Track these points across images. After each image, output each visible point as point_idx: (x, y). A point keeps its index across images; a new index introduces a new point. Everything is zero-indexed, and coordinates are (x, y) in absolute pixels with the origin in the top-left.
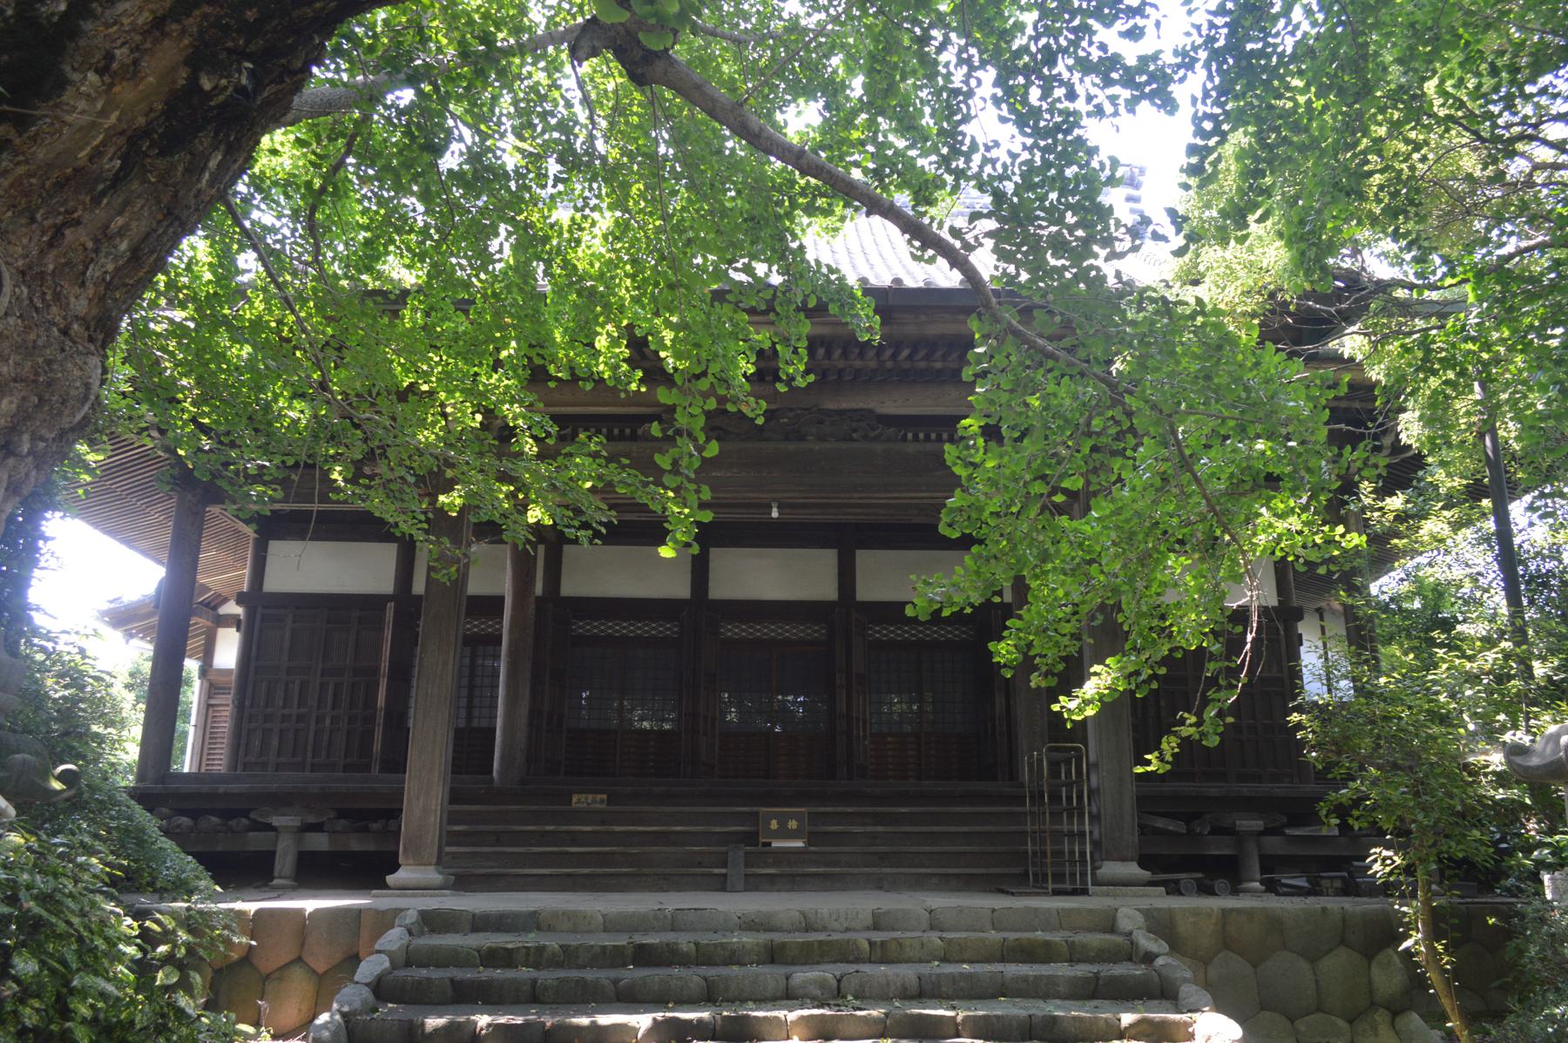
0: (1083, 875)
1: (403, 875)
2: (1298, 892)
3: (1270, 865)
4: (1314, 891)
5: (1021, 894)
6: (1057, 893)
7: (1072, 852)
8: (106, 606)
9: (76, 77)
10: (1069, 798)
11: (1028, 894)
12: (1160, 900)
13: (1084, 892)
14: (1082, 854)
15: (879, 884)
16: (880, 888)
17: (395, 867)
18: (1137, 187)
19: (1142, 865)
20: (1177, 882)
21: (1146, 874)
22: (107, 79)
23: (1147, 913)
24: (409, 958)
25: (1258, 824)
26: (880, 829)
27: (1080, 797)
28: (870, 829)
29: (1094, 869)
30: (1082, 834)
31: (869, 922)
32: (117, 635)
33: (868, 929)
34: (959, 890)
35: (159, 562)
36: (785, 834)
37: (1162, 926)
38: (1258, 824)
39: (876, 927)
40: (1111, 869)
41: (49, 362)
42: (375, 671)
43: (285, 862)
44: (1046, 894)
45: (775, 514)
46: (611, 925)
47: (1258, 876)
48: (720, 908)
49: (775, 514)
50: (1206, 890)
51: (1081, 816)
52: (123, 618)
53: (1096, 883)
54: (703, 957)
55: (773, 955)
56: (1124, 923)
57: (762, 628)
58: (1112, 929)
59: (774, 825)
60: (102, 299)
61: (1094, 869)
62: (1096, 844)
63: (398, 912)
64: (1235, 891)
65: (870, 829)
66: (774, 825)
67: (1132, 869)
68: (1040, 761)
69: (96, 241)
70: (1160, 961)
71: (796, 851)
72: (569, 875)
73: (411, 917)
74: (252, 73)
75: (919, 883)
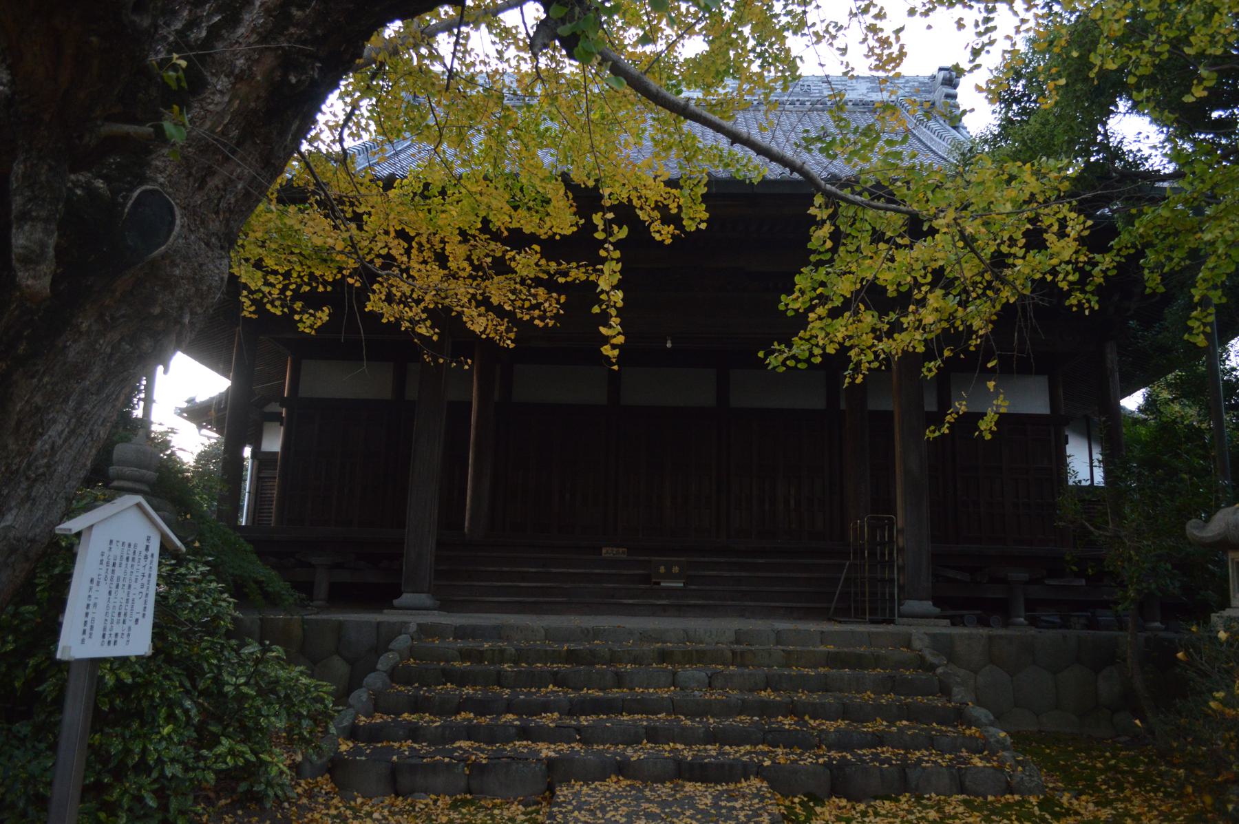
0: (892, 610)
1: (407, 598)
2: (1052, 625)
3: (1031, 605)
4: (1065, 625)
5: (845, 622)
6: (873, 622)
7: (884, 594)
8: (185, 405)
9: (215, 80)
10: (883, 554)
11: (852, 622)
12: (943, 628)
13: (891, 622)
14: (892, 595)
15: (742, 613)
16: (742, 616)
17: (399, 595)
18: (955, 87)
19: (935, 605)
20: (962, 616)
21: (938, 610)
22: (232, 79)
23: (933, 637)
24: (412, 652)
25: (1024, 576)
26: (743, 574)
27: (891, 554)
28: (735, 574)
29: (900, 605)
30: (892, 581)
31: (733, 638)
32: (191, 427)
33: (732, 643)
34: (800, 619)
35: (228, 377)
36: (669, 576)
37: (945, 647)
38: (1024, 576)
39: (738, 642)
40: (912, 605)
41: (201, 265)
42: (870, 634)
43: (322, 589)
44: (865, 623)
45: (669, 345)
46: (550, 634)
47: (1023, 614)
48: (627, 626)
49: (669, 345)
50: (983, 623)
51: (891, 567)
52: (198, 413)
53: (901, 616)
54: (613, 658)
55: (664, 656)
56: (917, 644)
57: (682, 388)
58: (908, 645)
59: (662, 569)
60: (228, 221)
61: (900, 605)
62: (901, 588)
63: (405, 624)
64: (1006, 624)
65: (735, 574)
66: (662, 569)
67: (927, 606)
68: (862, 527)
69: (225, 184)
70: (940, 670)
71: (676, 589)
72: (520, 602)
73: (413, 628)
74: (320, 69)
75: (769, 613)
